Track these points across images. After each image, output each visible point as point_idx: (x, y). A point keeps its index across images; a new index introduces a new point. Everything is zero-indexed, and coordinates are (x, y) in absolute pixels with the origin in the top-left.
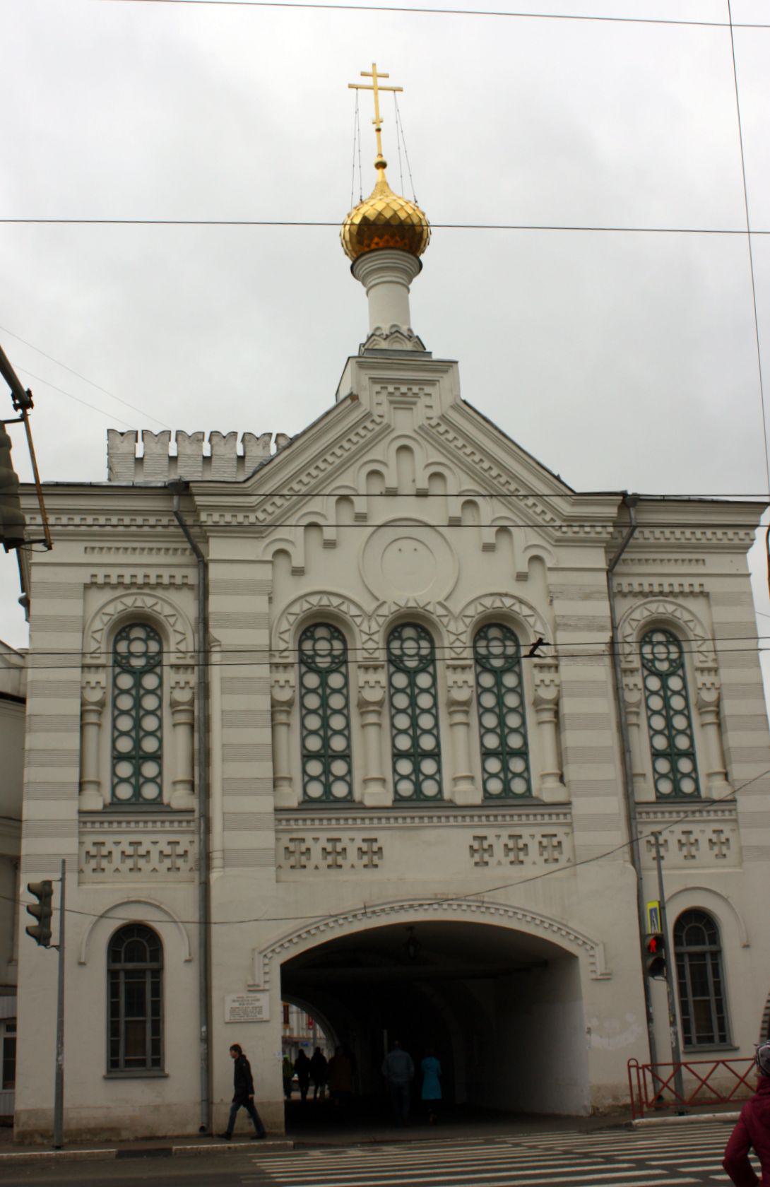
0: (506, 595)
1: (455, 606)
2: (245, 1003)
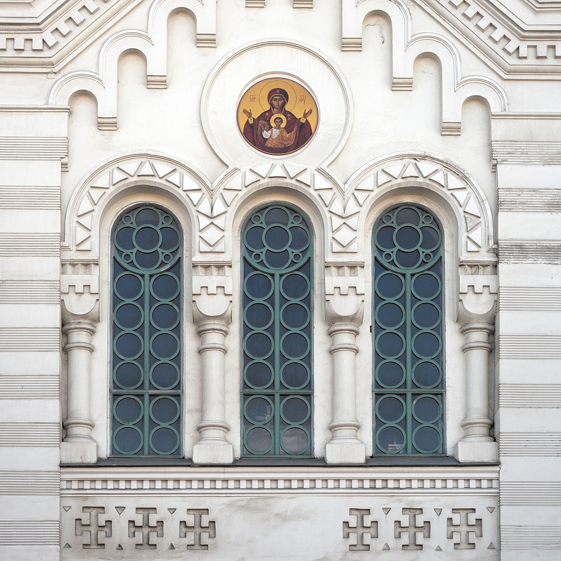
0: (424, 158)
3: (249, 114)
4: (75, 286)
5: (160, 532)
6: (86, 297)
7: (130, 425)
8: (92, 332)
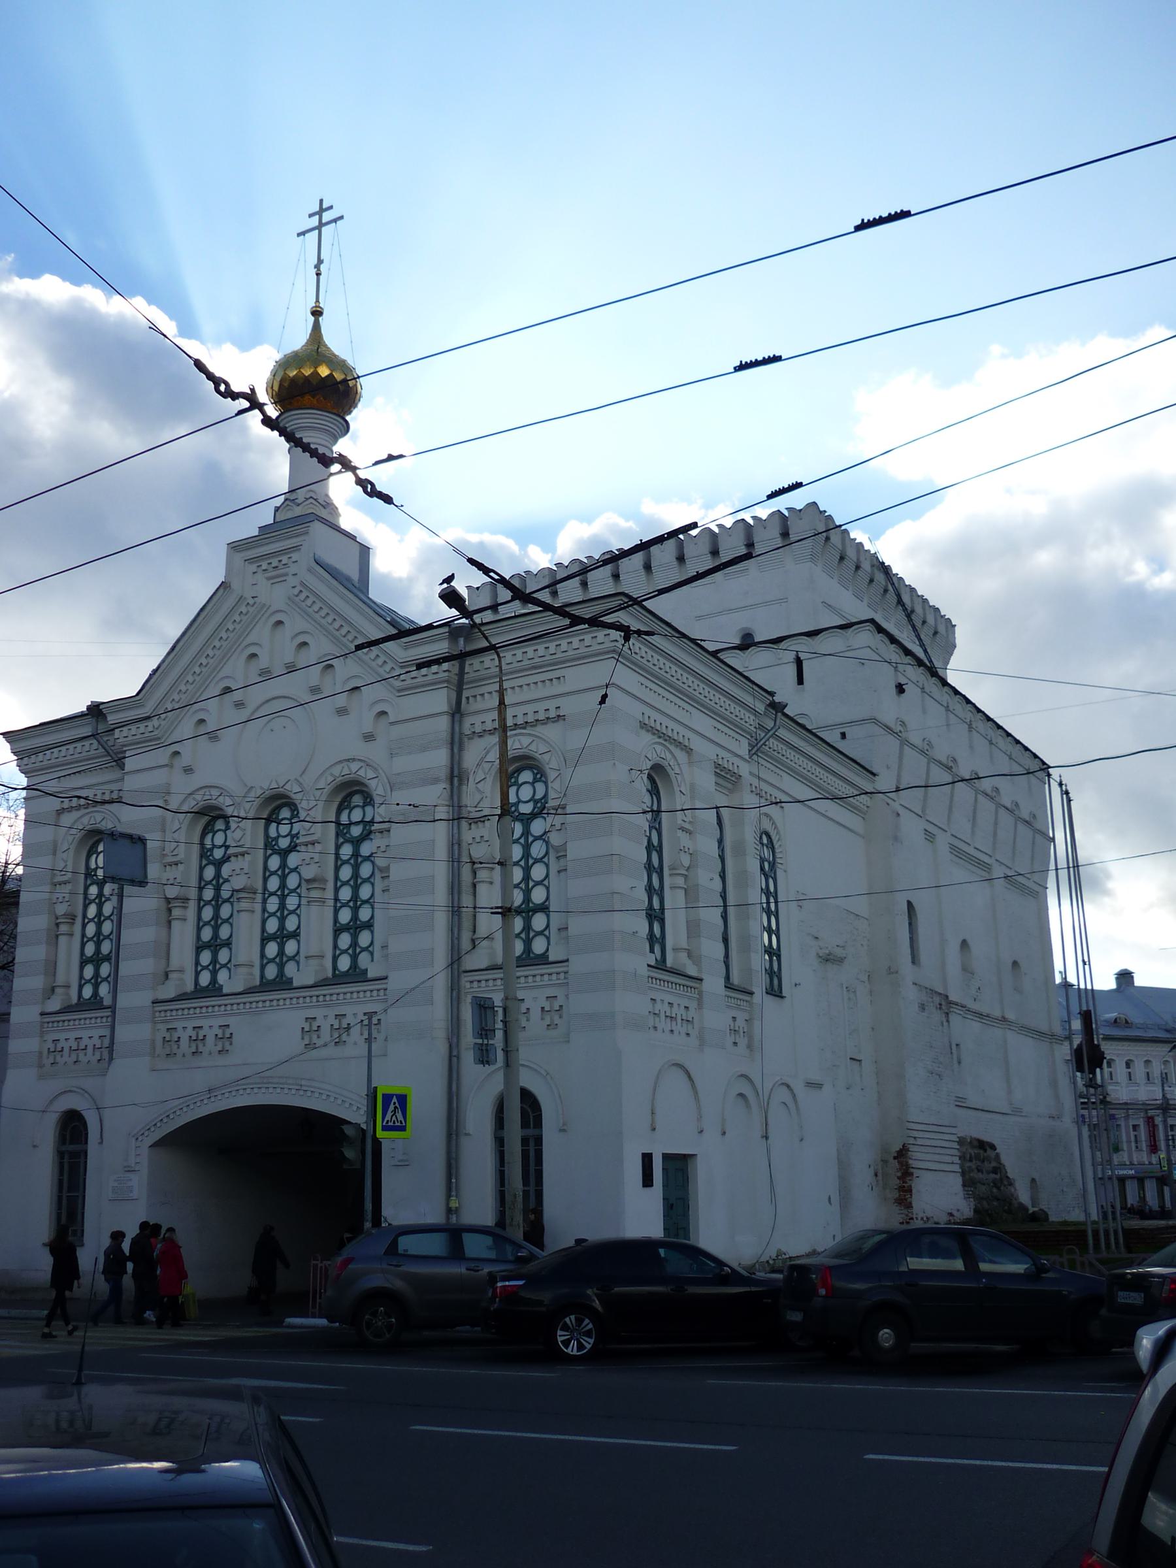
0: (354, 760)
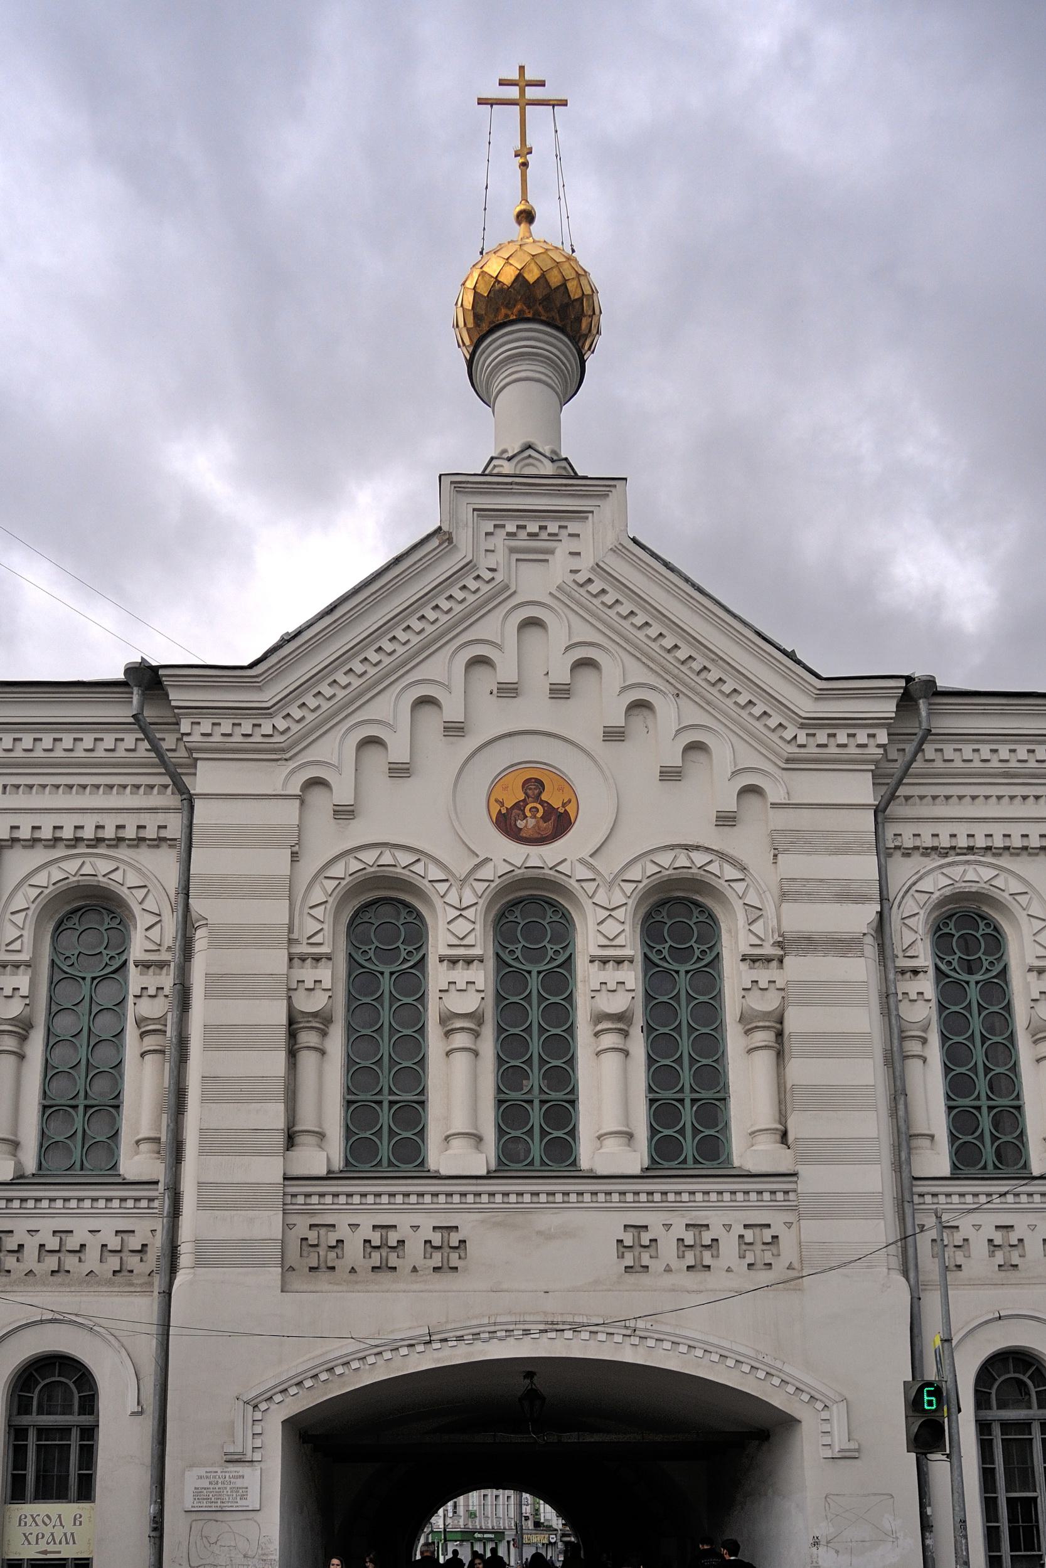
0: (697, 848)
1: (609, 866)
2: (220, 1481)
3: (502, 804)
4: (455, 983)
5: (401, 1253)
6: (921, 1003)
7: (367, 1135)
8: (324, 1034)
